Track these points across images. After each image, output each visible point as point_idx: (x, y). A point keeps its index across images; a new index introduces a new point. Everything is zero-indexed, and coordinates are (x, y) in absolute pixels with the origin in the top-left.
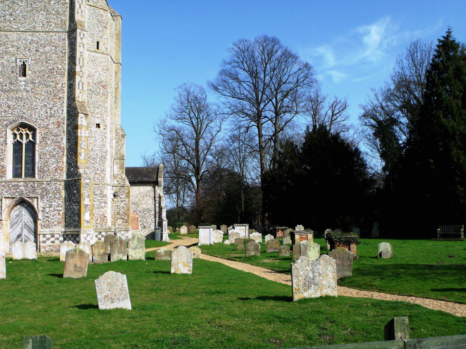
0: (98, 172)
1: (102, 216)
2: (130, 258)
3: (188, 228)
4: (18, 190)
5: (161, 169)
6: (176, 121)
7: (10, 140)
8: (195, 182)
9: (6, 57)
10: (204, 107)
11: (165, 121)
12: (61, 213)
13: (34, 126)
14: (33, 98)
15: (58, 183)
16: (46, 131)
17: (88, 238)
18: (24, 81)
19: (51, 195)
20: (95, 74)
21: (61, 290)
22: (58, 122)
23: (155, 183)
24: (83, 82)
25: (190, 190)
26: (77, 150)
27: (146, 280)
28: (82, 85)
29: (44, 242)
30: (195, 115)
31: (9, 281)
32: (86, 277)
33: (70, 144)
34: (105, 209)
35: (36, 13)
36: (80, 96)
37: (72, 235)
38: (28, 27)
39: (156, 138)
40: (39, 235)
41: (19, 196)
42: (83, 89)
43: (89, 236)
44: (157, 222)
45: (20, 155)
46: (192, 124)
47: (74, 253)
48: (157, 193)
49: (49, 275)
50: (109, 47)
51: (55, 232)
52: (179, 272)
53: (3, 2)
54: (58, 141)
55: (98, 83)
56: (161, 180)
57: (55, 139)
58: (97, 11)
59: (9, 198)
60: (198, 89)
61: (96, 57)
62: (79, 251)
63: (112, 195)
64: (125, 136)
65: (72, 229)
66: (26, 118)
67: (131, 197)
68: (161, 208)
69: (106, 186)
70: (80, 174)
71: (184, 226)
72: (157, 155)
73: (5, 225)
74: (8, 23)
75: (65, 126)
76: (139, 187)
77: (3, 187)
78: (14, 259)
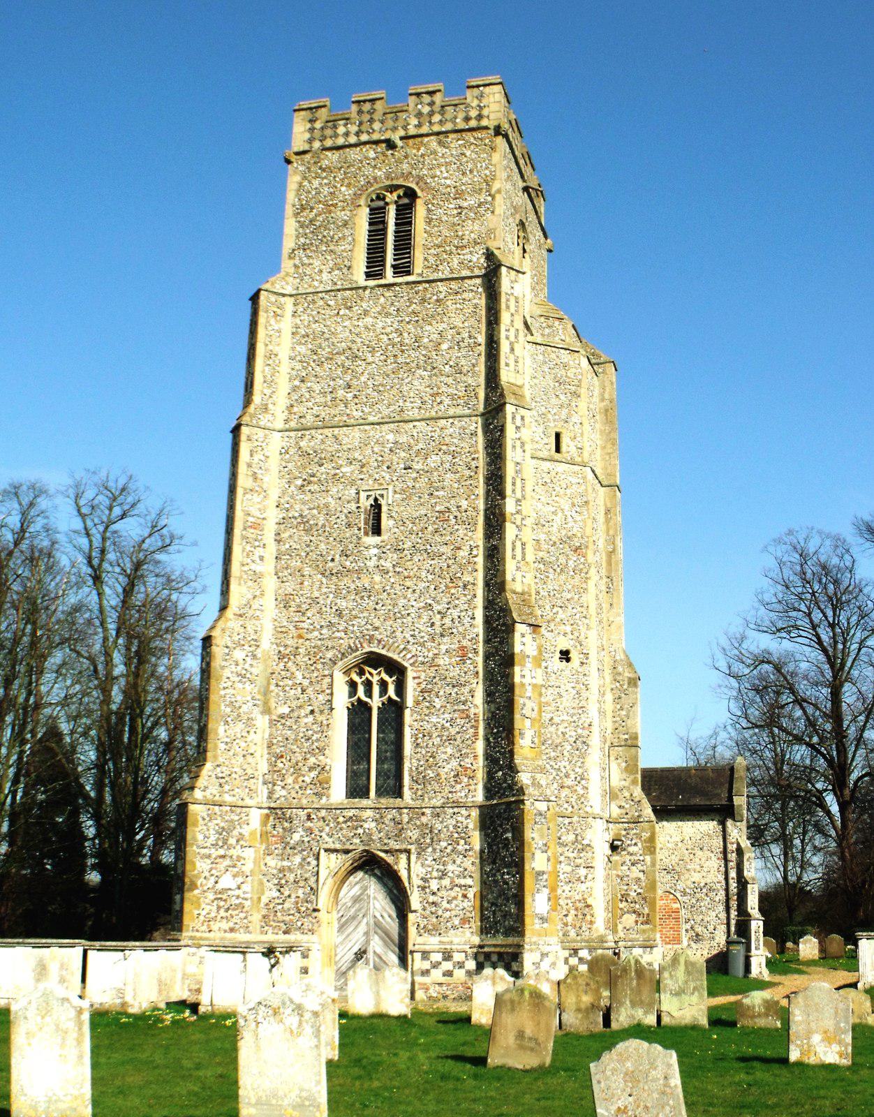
0: (568, 782)
1: (580, 905)
2: (666, 1020)
3: (820, 943)
4: (360, 831)
5: (740, 773)
6: (772, 636)
7: (342, 700)
8: (835, 809)
9: (335, 490)
10: (851, 593)
11: (743, 638)
12: (471, 895)
13: (399, 660)
14: (399, 588)
15: (463, 811)
16: (432, 672)
17: (545, 965)
18: (378, 547)
19: (444, 844)
20: (554, 517)
21: (487, 1097)
22: (462, 648)
23: (725, 813)
24: (524, 540)
25: (820, 830)
26: (512, 721)
27: (720, 1079)
28: (523, 549)
29: (426, 973)
30: (826, 617)
31: (346, 1067)
32: (550, 1066)
33: (492, 706)
34: (588, 884)
35: (406, 375)
36: (519, 579)
37: (500, 955)
38: (386, 412)
39: (720, 686)
40: (412, 952)
41: (362, 848)
42: (523, 558)
43: (546, 959)
44: (733, 922)
45: (364, 738)
46: (820, 642)
47: (516, 999)
48: (730, 839)
49: (447, 1057)
50: (586, 445)
51: (453, 947)
52: (812, 1060)
53: (331, 359)
54: (463, 699)
55: (562, 542)
56: (740, 801)
57: (453, 695)
58: (553, 356)
59: (336, 851)
60: (828, 542)
61: (553, 473)
62: (531, 994)
63: (607, 845)
64: (639, 683)
65: (500, 940)
66: (379, 641)
67: (658, 850)
68: (743, 884)
69: (590, 819)
70: (522, 788)
71: (808, 937)
72: (723, 736)
73: (324, 925)
74: (342, 407)
75: (480, 659)
76: (680, 823)
77: (321, 823)
78: (350, 1013)
